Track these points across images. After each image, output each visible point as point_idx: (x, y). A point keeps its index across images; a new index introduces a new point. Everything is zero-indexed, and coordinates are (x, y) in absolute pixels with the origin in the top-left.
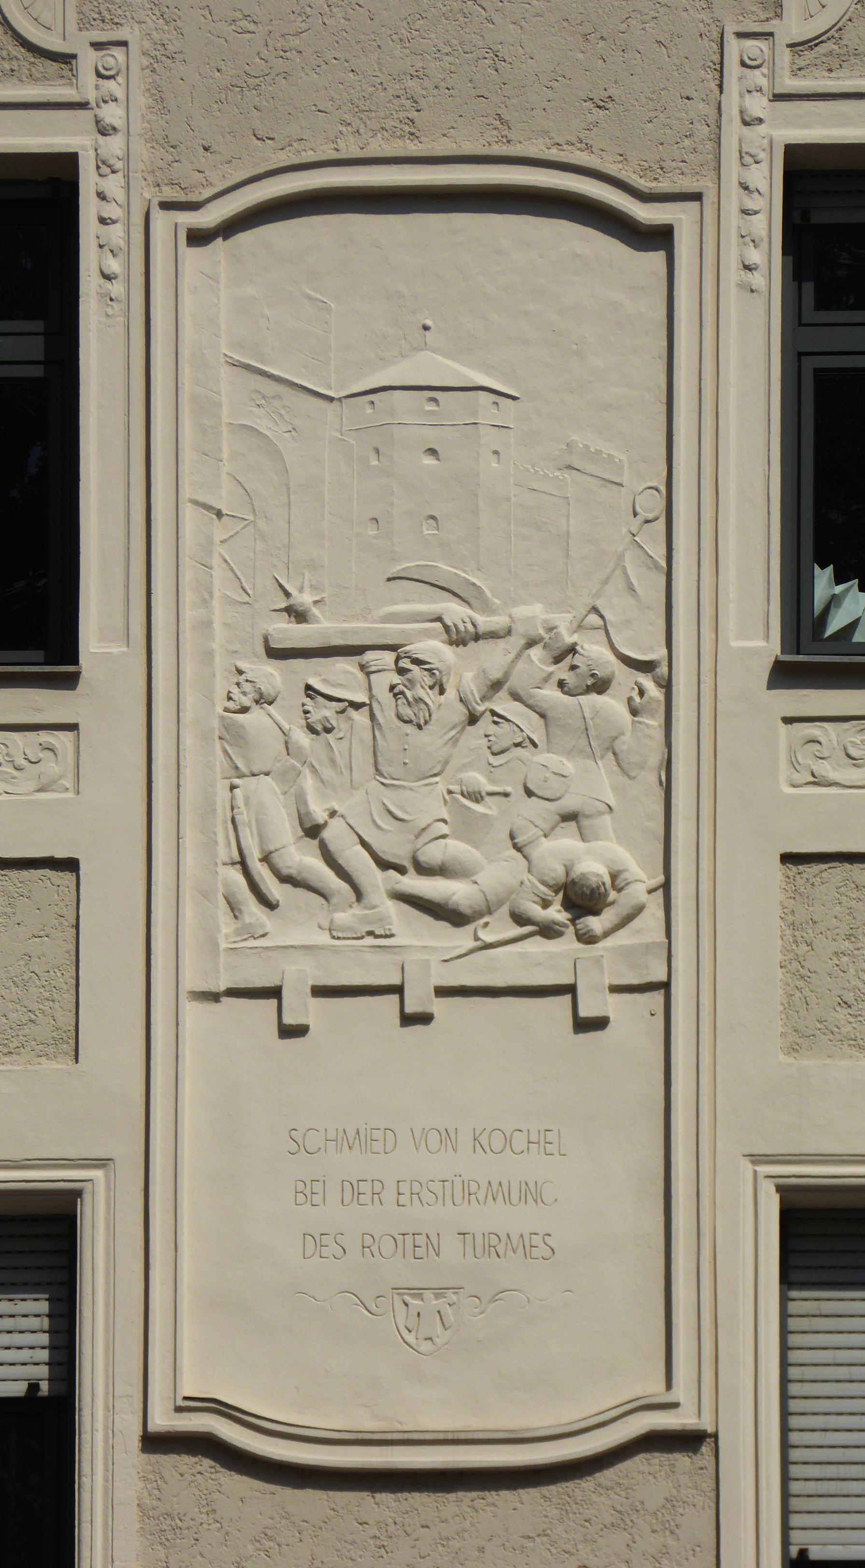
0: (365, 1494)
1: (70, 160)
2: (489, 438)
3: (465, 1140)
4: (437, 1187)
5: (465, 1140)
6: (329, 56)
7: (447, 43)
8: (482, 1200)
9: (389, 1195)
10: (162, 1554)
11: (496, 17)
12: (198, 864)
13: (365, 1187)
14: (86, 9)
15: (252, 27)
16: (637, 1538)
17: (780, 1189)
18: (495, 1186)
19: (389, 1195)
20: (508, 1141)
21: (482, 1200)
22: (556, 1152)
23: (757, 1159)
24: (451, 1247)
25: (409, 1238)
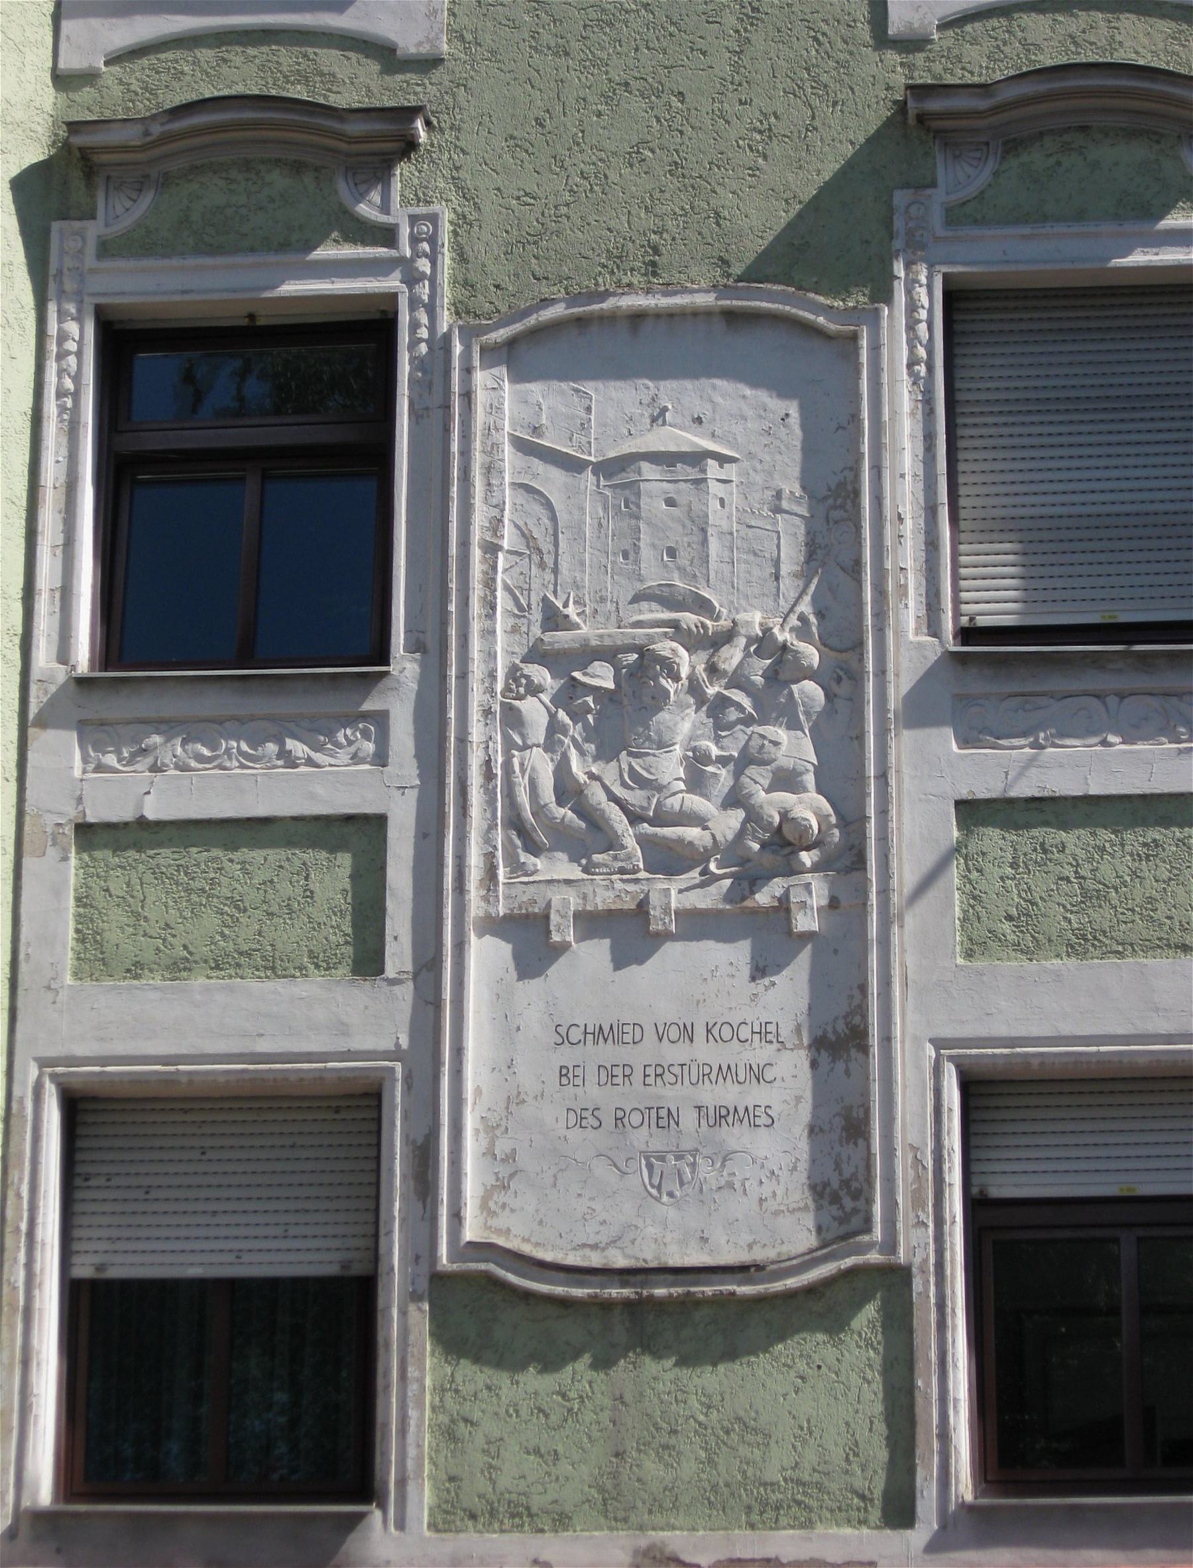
0: (688, 384)
1: (393, 297)
2: (715, 488)
3: (700, 1032)
4: (676, 1070)
5: (700, 1032)
6: (591, 220)
7: (682, 209)
8: (714, 1080)
9: (638, 1076)
10: (449, 1370)
11: (718, 189)
12: (478, 838)
13: (618, 1071)
14: (406, 193)
15: (532, 201)
16: (846, 1353)
17: (957, 1067)
18: (725, 1069)
19: (638, 1076)
20: (735, 1033)
21: (714, 1080)
22: (775, 1040)
23: (939, 1044)
24: (688, 1119)
25: (653, 1113)
